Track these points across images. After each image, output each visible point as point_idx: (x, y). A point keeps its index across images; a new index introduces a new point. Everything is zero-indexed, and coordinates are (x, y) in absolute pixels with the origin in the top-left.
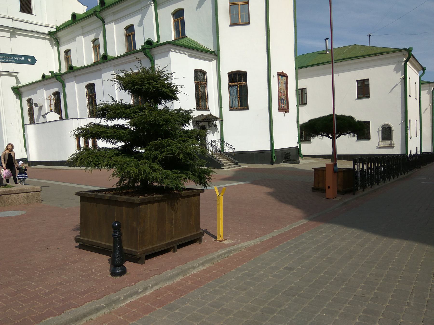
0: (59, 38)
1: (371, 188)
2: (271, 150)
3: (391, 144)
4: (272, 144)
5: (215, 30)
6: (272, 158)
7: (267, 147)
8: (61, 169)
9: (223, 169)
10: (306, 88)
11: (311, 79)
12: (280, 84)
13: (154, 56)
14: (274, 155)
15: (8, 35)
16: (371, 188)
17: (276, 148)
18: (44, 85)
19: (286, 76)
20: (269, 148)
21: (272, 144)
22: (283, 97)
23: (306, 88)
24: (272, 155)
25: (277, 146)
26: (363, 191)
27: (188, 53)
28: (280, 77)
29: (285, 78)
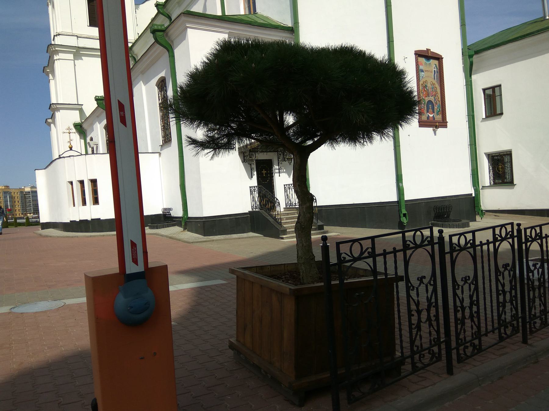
0: (136, 55)
1: (525, 341)
2: (398, 202)
3: (507, 155)
4: (400, 191)
5: (390, 28)
6: (400, 217)
7: (393, 197)
8: (72, 237)
9: (282, 238)
10: (500, 86)
11: (509, 67)
12: (422, 74)
13: (172, 42)
14: (404, 211)
15: (71, 56)
16: (525, 341)
17: (407, 198)
18: (98, 117)
19: (439, 59)
20: (394, 198)
21: (400, 191)
22: (432, 98)
23: (500, 86)
24: (400, 211)
25: (409, 196)
26: (450, 371)
27: (228, 31)
28: (422, 60)
29: (436, 62)
